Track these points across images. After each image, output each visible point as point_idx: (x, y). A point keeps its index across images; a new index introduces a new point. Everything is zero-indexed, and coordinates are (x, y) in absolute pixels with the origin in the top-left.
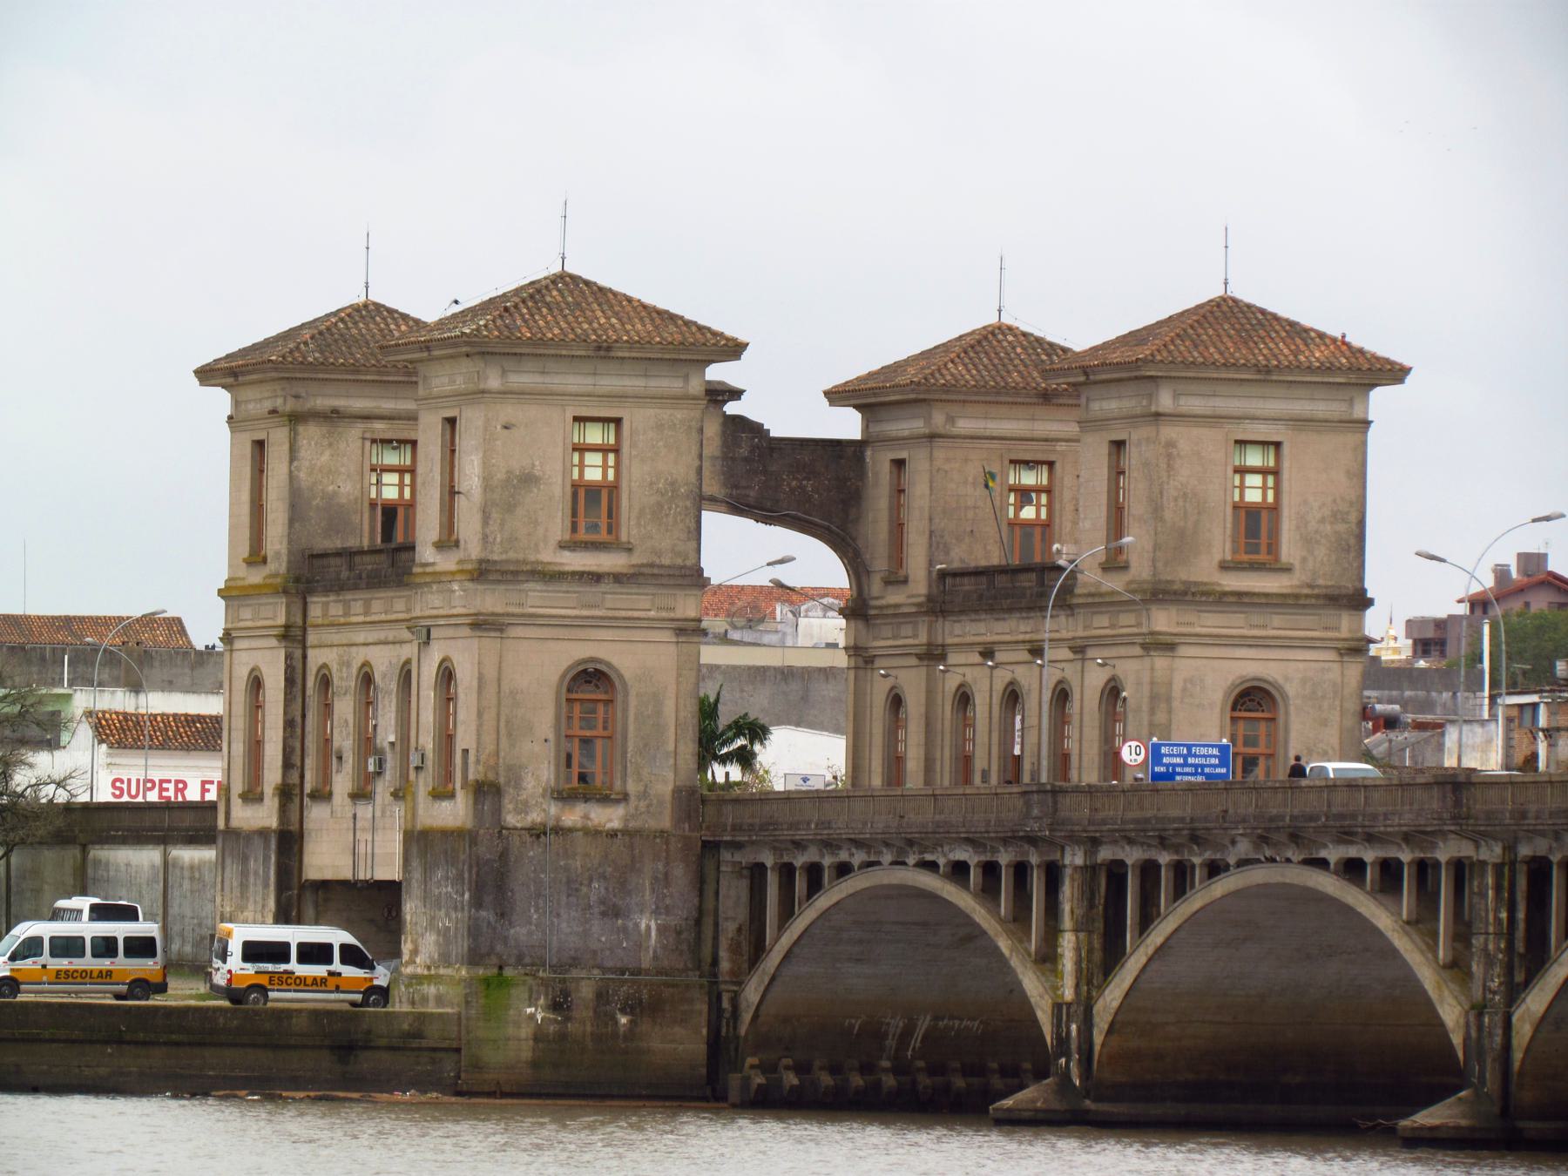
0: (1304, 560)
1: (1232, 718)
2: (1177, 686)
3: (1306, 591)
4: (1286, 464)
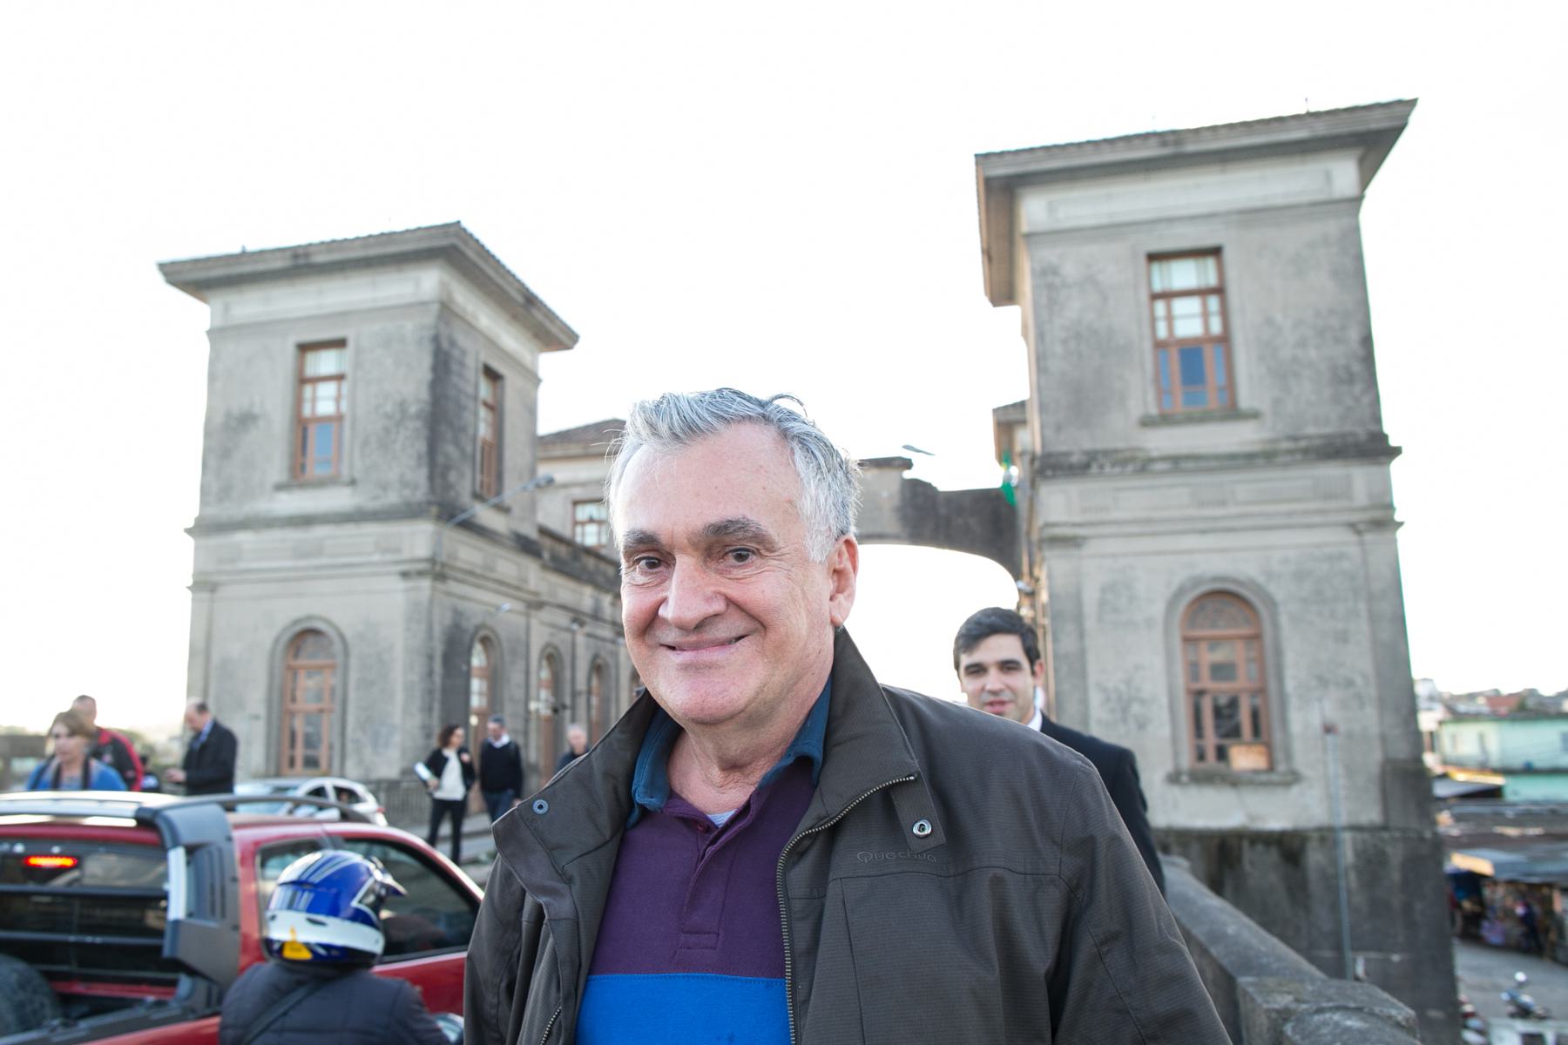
0: (1277, 402)
1: (1187, 640)
2: (1091, 597)
3: (1285, 445)
4: (1232, 274)
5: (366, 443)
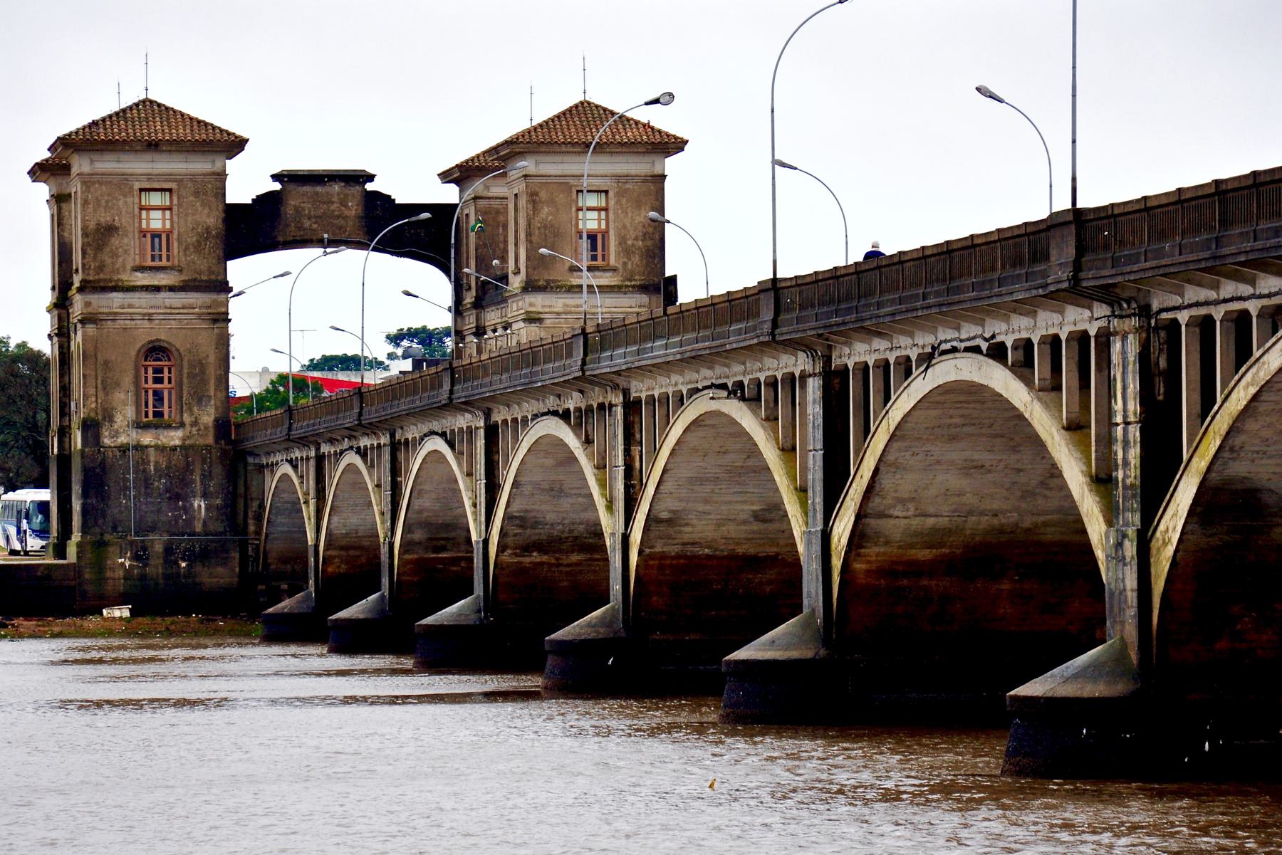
0: (625, 264)
4: (612, 203)
5: (186, 249)
